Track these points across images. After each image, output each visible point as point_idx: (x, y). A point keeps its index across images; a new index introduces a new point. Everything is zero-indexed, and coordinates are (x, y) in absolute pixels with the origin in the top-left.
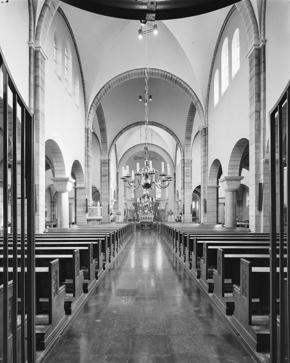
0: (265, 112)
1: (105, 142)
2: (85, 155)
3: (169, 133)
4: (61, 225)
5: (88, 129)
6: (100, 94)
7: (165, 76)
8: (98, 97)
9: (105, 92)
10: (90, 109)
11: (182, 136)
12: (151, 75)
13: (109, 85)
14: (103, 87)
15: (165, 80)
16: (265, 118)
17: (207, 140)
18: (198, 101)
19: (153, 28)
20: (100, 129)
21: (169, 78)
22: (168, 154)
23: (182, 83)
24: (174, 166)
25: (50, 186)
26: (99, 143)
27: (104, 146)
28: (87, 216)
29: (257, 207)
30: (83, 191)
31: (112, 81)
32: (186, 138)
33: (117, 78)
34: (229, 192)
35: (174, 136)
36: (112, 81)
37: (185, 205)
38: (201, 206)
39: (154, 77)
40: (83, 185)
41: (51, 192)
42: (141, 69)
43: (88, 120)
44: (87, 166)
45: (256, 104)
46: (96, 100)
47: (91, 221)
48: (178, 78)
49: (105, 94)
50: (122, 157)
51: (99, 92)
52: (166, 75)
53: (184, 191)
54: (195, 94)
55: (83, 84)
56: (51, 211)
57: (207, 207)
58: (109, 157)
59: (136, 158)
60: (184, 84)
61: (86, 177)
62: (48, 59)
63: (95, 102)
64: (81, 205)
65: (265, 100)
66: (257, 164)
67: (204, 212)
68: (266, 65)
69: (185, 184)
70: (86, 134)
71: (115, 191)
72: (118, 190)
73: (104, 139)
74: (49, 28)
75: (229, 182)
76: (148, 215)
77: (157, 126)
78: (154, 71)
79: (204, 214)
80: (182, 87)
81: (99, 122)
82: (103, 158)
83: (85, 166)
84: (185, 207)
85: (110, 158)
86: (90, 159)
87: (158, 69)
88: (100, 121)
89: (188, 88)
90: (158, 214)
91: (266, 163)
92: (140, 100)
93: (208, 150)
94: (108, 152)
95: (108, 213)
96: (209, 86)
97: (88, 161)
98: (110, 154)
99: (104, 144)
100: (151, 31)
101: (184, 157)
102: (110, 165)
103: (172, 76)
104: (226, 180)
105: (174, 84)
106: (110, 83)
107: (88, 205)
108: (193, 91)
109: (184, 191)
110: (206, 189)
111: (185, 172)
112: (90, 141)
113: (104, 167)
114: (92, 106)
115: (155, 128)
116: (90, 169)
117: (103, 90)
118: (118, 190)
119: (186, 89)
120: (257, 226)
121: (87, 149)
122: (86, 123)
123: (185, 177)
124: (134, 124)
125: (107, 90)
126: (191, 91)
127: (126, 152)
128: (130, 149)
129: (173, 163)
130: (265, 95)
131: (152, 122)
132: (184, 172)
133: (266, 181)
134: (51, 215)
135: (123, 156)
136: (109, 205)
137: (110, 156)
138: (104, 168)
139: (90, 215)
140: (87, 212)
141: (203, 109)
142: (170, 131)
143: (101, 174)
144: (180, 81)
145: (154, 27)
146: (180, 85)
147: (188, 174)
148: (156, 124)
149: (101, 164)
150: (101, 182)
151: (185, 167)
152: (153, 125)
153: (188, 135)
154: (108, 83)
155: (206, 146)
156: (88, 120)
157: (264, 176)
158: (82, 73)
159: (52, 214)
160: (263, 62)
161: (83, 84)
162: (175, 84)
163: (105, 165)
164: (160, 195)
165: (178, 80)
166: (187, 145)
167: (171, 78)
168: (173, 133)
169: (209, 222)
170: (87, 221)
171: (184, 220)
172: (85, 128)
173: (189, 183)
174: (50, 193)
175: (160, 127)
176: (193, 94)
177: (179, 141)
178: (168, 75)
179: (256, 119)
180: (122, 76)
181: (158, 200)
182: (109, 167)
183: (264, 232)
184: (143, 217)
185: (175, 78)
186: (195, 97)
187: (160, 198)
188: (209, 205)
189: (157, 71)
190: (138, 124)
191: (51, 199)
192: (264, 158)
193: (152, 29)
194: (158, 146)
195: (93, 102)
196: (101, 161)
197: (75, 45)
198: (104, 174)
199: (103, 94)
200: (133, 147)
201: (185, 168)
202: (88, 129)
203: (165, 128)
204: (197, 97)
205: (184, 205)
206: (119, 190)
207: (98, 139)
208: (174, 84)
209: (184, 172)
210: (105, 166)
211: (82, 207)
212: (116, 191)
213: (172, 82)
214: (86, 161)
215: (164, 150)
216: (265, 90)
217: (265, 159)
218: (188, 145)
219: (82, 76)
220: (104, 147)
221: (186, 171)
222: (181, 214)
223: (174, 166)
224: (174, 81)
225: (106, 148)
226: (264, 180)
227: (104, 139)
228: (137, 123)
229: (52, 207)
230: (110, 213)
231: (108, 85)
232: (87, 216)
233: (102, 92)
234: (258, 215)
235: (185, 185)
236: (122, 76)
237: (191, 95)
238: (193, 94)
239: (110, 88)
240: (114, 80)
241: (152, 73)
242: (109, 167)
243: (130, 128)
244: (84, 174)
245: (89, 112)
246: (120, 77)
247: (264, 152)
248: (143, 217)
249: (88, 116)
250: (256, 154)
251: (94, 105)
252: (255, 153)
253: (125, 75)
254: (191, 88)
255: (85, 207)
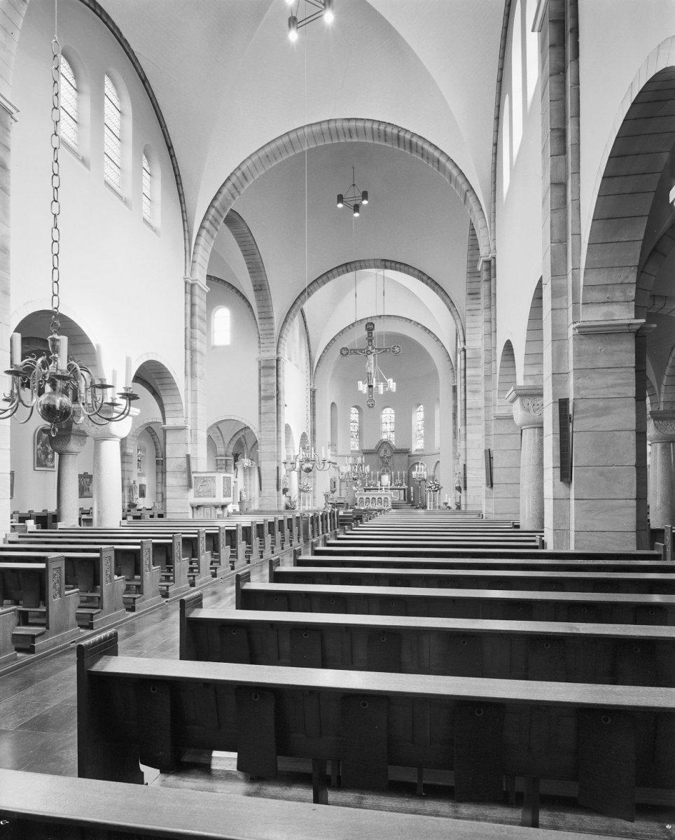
0: (579, 183)
1: (267, 317)
2: (186, 349)
3: (427, 284)
4: (100, 520)
5: (192, 285)
6: (221, 197)
7: (382, 134)
8: (217, 204)
9: (234, 191)
10: (199, 235)
11: (458, 290)
12: (348, 136)
13: (243, 174)
14: (229, 179)
15: (384, 144)
16: (579, 199)
17: (493, 292)
18: (468, 191)
19: (323, 7)
20: (254, 286)
21: (392, 137)
22: (438, 340)
23: (426, 146)
24: (452, 369)
25: (151, 425)
26: (255, 319)
27: (267, 327)
28: (191, 498)
29: (558, 472)
30: (180, 435)
31: (249, 163)
32: (469, 294)
33: (261, 154)
34: (532, 430)
35: (440, 290)
36: (249, 163)
37: (468, 466)
38: (197, 472)
39: (355, 140)
40: (179, 422)
41: (156, 440)
42: (320, 123)
43: (194, 262)
44: (191, 373)
45: (552, 160)
46: (213, 211)
47: (202, 508)
48: (414, 135)
49: (237, 198)
50: (324, 352)
51: (219, 192)
52: (385, 131)
53: (465, 430)
54: (461, 172)
55: (177, 176)
56: (157, 483)
57: (495, 471)
58: (278, 353)
59: (344, 352)
60: (431, 150)
61: (187, 401)
62: (18, 111)
63: (210, 217)
64: (176, 470)
65: (577, 145)
66: (557, 343)
67: (487, 484)
68: (581, 40)
69: (467, 411)
70: (189, 296)
71: (304, 435)
72: (314, 432)
73: (265, 310)
74: (17, 35)
75: (527, 400)
76: (379, 492)
77: (396, 269)
78: (353, 124)
79: (489, 489)
80: (428, 158)
81: (249, 268)
82: (266, 355)
83: (186, 375)
84: (468, 472)
85: (280, 355)
86: (198, 358)
87: (362, 119)
88: (250, 266)
89: (443, 159)
90: (417, 490)
91: (582, 337)
92: (340, 205)
93: (495, 319)
94: (275, 340)
95: (276, 487)
96: (496, 145)
97: (193, 362)
98: (281, 346)
99: (265, 321)
100: (317, 16)
101: (465, 344)
102: (281, 373)
103: (399, 132)
104: (518, 395)
105: (409, 153)
106: (244, 168)
107: (193, 469)
108: (456, 165)
109: (465, 430)
110: (492, 424)
111: (467, 382)
112: (197, 314)
113: (265, 376)
114: (202, 227)
115: (390, 274)
116: (199, 382)
117: (229, 185)
118: (314, 432)
119: (438, 161)
120: (560, 531)
121: (191, 333)
122: (189, 269)
123: (467, 393)
124: (337, 268)
125: (238, 185)
126: (449, 166)
127: (333, 339)
128: (342, 332)
129: (450, 360)
130: (579, 131)
131: (382, 260)
132: (465, 382)
133: (582, 392)
134: (157, 493)
135: (326, 348)
136: (278, 468)
137: (281, 350)
138: (266, 379)
139: (198, 495)
140: (190, 486)
141: (481, 209)
142: (429, 278)
143: (260, 395)
144: (420, 143)
145: (324, 4)
146: (423, 153)
147: (475, 387)
148: (398, 266)
149: (260, 370)
150: (260, 413)
151: (467, 369)
152: (386, 268)
153: (474, 285)
154: (239, 168)
155: (493, 308)
156: (194, 262)
157: (576, 378)
158: (170, 148)
159: (160, 490)
160: (571, 31)
161: (177, 176)
162: (411, 152)
163: (270, 371)
164: (422, 441)
165: (414, 140)
166: (472, 313)
167: (398, 137)
168: (436, 284)
169: (500, 511)
170: (192, 507)
171: (466, 505)
172: (186, 283)
173: (480, 409)
174: (155, 443)
175: (408, 273)
176: (455, 172)
177: (452, 302)
178: (389, 129)
179: (554, 208)
180: (273, 146)
181: (417, 455)
182: (277, 376)
183: (554, 548)
184: (365, 497)
185: (408, 136)
186: (460, 180)
187: (422, 450)
188: (499, 465)
189: (360, 124)
190: (348, 267)
191: (157, 457)
192: (574, 323)
193: (320, 9)
194: (411, 321)
195: (205, 218)
196: (260, 362)
197: (144, 81)
198: (266, 394)
199: (230, 198)
200: (349, 327)
201: (468, 372)
202: (192, 285)
203: (416, 272)
204: (466, 179)
205: (465, 465)
206: (317, 433)
207: (250, 306)
208: (408, 152)
209: (465, 382)
210: (269, 376)
211: (179, 475)
212: (309, 435)
213: (402, 149)
214: (189, 363)
215: (426, 329)
216: (577, 115)
217: (578, 324)
218: (475, 312)
219: (172, 156)
220: (265, 328)
221: (472, 378)
222: (459, 489)
223: (452, 369)
224: (408, 145)
225: (271, 332)
226: (577, 389)
227: (265, 310)
228: (346, 264)
229: (160, 475)
230: (282, 487)
231: (239, 173)
232: (191, 498)
233: (225, 191)
234: (562, 495)
235: (467, 416)
236: (273, 146)
237: (451, 176)
238: (455, 172)
239: (246, 180)
240: (255, 158)
241: (350, 131)
242: (277, 376)
243: (329, 280)
244: (182, 396)
245: (196, 244)
246: (267, 149)
247: (575, 303)
248: (365, 497)
249: (194, 253)
250: (555, 312)
251: (207, 224)
252: (552, 309)
253: (279, 143)
254: (449, 159)
255: (185, 476)
